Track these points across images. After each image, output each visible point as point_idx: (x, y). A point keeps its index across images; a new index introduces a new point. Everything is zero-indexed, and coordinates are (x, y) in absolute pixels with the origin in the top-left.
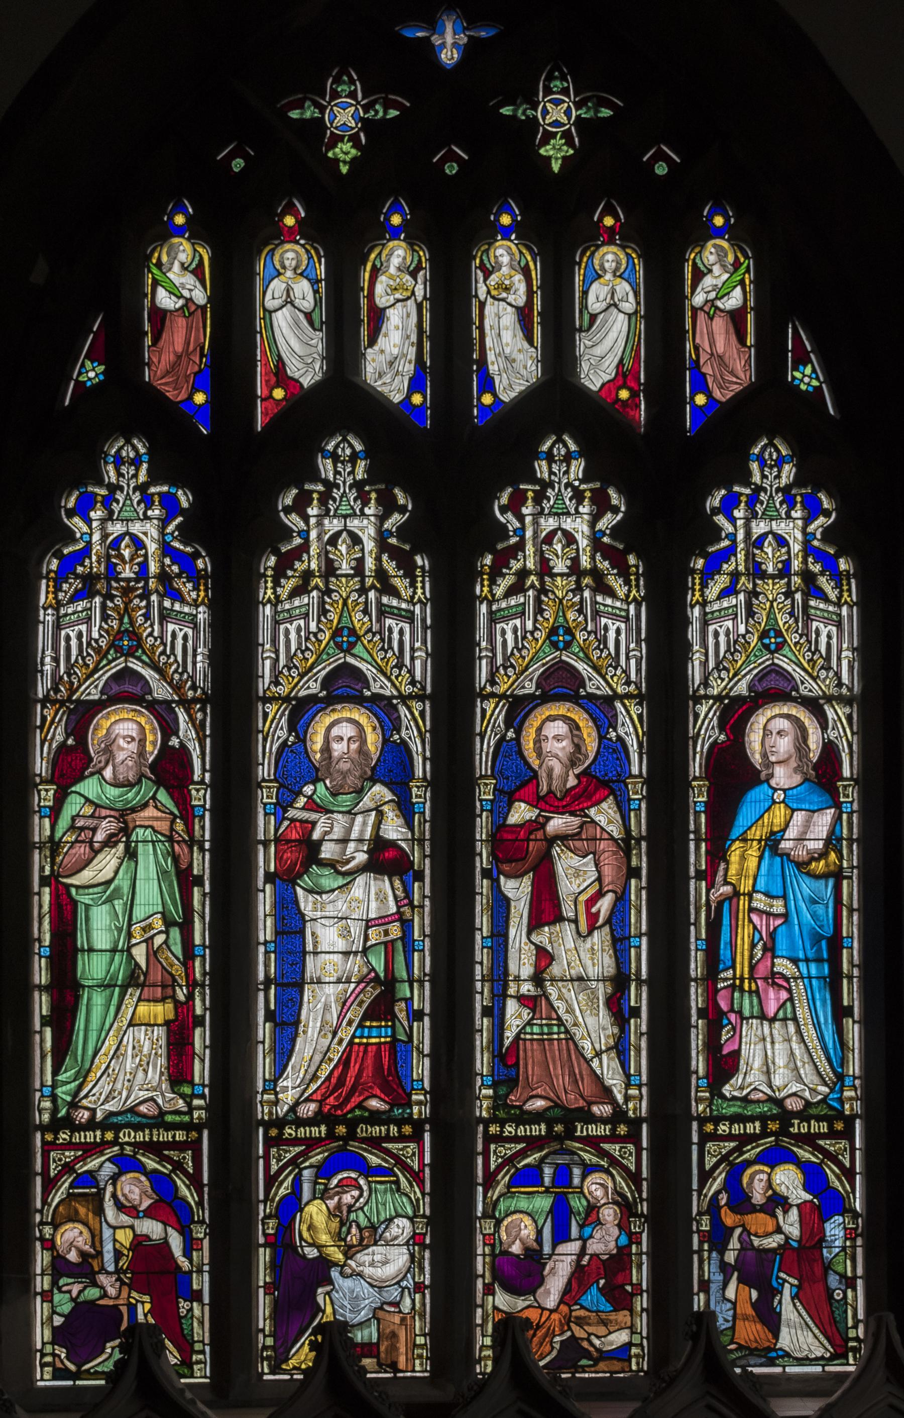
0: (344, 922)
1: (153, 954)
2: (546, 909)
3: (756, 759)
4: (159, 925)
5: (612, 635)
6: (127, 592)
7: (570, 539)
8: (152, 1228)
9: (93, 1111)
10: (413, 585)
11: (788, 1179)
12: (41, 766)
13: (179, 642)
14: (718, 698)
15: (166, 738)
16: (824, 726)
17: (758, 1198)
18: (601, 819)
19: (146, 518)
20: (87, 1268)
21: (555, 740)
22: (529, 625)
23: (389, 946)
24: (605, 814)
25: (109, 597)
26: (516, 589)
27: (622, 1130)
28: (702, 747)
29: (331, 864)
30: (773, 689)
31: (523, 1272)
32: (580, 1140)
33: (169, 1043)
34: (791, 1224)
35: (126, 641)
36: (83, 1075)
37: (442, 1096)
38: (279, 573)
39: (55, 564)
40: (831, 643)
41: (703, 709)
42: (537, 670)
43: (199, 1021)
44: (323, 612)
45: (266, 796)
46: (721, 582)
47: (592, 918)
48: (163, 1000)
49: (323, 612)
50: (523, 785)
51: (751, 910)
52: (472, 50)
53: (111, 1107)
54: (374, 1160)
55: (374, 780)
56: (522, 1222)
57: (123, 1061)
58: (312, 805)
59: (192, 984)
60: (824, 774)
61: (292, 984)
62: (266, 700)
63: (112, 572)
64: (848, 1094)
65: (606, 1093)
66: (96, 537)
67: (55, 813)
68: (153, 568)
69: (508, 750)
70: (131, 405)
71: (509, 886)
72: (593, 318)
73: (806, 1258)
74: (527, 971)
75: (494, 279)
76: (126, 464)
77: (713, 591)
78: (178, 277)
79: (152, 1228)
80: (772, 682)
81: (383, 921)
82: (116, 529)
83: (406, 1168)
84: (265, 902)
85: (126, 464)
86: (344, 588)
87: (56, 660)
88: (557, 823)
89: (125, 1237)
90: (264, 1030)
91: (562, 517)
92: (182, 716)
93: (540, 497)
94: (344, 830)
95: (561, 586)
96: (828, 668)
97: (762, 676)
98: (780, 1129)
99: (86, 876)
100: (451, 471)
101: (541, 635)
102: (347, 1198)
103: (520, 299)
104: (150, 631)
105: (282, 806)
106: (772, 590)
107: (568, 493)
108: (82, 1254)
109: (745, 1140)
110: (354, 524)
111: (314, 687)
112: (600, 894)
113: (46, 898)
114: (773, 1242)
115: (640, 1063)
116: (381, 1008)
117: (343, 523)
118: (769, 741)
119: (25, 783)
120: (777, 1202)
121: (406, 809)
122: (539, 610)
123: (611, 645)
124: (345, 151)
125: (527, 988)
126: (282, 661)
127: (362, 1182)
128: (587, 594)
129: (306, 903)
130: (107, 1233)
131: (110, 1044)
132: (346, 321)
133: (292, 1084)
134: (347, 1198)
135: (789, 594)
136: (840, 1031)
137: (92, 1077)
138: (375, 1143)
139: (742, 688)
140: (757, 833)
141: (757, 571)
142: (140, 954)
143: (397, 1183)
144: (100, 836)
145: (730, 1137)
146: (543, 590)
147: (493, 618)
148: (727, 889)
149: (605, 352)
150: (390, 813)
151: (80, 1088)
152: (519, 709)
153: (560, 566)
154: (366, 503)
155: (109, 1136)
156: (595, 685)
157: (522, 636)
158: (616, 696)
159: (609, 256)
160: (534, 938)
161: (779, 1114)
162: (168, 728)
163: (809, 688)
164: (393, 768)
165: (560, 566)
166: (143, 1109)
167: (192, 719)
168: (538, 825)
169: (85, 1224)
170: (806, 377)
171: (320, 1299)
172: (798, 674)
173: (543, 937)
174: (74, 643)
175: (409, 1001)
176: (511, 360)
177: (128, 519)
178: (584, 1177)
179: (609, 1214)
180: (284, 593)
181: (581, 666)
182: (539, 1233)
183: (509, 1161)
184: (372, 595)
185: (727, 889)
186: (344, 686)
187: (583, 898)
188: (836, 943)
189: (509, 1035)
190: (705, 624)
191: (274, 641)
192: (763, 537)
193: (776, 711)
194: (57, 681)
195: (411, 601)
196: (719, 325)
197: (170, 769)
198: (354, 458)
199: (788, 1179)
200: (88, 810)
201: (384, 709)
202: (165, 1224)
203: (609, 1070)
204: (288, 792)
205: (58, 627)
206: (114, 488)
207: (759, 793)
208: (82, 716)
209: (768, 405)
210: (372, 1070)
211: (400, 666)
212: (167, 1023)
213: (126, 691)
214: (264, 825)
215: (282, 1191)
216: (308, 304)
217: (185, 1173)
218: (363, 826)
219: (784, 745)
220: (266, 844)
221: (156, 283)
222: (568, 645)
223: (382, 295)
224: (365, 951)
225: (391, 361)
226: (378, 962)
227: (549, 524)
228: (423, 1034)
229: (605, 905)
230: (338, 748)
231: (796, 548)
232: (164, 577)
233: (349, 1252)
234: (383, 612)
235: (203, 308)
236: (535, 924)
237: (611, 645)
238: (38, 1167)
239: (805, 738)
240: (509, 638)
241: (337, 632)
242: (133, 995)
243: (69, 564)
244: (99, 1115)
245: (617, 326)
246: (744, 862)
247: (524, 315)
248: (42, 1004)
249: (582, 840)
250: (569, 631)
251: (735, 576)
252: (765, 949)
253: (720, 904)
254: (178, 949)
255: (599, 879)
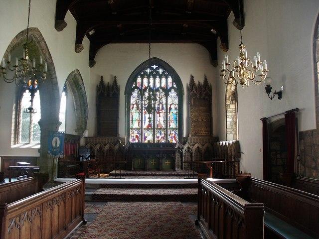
11: (173, 132)
20: (133, 137)
24: (163, 110)
30: (173, 104)
31: (158, 137)
56: (158, 135)
70: (136, 87)
73: (174, 137)
132: (149, 82)
161: (173, 129)
170: (175, 86)
176: (158, 85)
199: (173, 132)
209: (173, 87)
210: (150, 125)
225: (151, 85)
246: (171, 114)
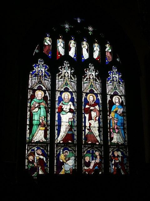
0: (66, 118)
1: (42, 121)
2: (90, 118)
3: (114, 102)
4: (43, 117)
5: (97, 86)
6: (40, 77)
7: (93, 75)
8: (42, 157)
9: (34, 141)
10: (75, 79)
11: (119, 153)
12: (29, 97)
13: (47, 83)
14: (110, 95)
15: (45, 95)
16: (122, 99)
17: (116, 155)
18: (97, 108)
19: (43, 68)
21: (91, 98)
22: (88, 84)
23: (72, 122)
24: (97, 107)
25: (38, 77)
26: (87, 80)
27: (100, 146)
28: (58, 96)
29: (65, 111)
31: (88, 164)
32: (95, 147)
33: (44, 132)
34: (120, 159)
35: (40, 82)
36: (33, 136)
37: (77, 140)
38: (59, 76)
39: (32, 72)
40: (121, 89)
41: (108, 96)
42: (89, 90)
43: (48, 130)
44: (64, 81)
45: (57, 103)
46: (110, 81)
47: (96, 120)
48: (43, 127)
49: (64, 81)
50: (88, 103)
51: (114, 120)
52: (81, 21)
53: (37, 140)
54: (70, 149)
55: (70, 101)
57: (39, 135)
58: (62, 104)
59: (47, 125)
60: (121, 104)
61: (60, 126)
62: (57, 91)
63: (38, 74)
64: (126, 143)
65: (98, 141)
66: (37, 70)
67: (30, 103)
68: (44, 74)
69: (86, 99)
71: (86, 115)
72: (95, 51)
74: (88, 126)
75: (84, 46)
76: (41, 62)
77: (109, 83)
78: (48, 41)
79: (42, 157)
80: (116, 93)
81: (71, 118)
82: (39, 69)
83: (74, 150)
84: (57, 115)
85: (41, 62)
86: (67, 78)
87: (31, 84)
88: (92, 108)
89: (38, 158)
90: (56, 132)
91: (91, 73)
92: (47, 92)
93: (89, 70)
94: (66, 108)
95: (92, 80)
96: (122, 92)
97: (115, 92)
98: (118, 146)
99: (34, 111)
100: (79, 67)
101: (89, 86)
102: (66, 154)
103: (87, 48)
104: (43, 81)
105: (59, 103)
106: (115, 83)
107: (92, 70)
108: (32, 160)
109: (114, 148)
110: (68, 71)
111: (63, 90)
112: (97, 117)
113: (29, 113)
114: (118, 161)
115: (102, 138)
116: (70, 130)
117: (66, 71)
118: (116, 100)
119: (27, 99)
120: (118, 156)
121: (74, 105)
122: (89, 83)
123: (97, 87)
124: (67, 30)
125: (88, 128)
126: (59, 86)
127: (68, 152)
128: (95, 81)
129: (61, 115)
130: (35, 157)
131: (37, 132)
133: (59, 139)
134: (66, 154)
135: (117, 83)
136: (125, 135)
137: (34, 137)
138: (70, 147)
139: (112, 94)
140: (114, 110)
141: (113, 80)
142: (41, 121)
143: (73, 152)
144: (36, 106)
145: (113, 148)
146: (89, 81)
147: (84, 83)
148: (111, 117)
149: (96, 55)
150: (72, 105)
151: (33, 138)
152: (87, 94)
153: (91, 78)
154: (69, 69)
155: (36, 144)
156: (96, 92)
157: (87, 86)
158: (98, 93)
159: (60, 40)
160: (89, 122)
162: (45, 93)
163: (120, 94)
164: (72, 100)
165: (91, 78)
166: (41, 141)
167: (48, 92)
168: (89, 108)
169: (33, 156)
171: (63, 167)
172: (118, 93)
173: (90, 121)
174: (34, 82)
175: (74, 129)
176: (86, 55)
177: (41, 68)
178: (95, 152)
179: (98, 157)
180: (59, 78)
181: (94, 90)
182: (90, 159)
183: (87, 150)
184: (70, 79)
185: (111, 117)
186: (66, 90)
187: (95, 117)
188: (124, 124)
189: (86, 134)
190: (108, 86)
191: (58, 84)
192: (114, 77)
193: (116, 96)
194: (31, 86)
195: (74, 80)
196: (108, 53)
197: (45, 98)
198: (68, 64)
199: (119, 153)
200: (35, 102)
201: (71, 93)
202: (43, 156)
203: (98, 138)
204: (59, 102)
205: (32, 80)
206: (39, 64)
207: (115, 106)
208: (34, 91)
210: (68, 136)
211: (73, 88)
212: (44, 130)
213: (40, 89)
214: (57, 106)
215: (58, 153)
216: (63, 46)
217: (46, 150)
218: (68, 107)
219: (117, 101)
220: (57, 108)
221: (45, 42)
222: (92, 87)
223: (71, 46)
224: (69, 122)
226: (70, 123)
227: (90, 73)
228: (76, 133)
229: (97, 118)
230: (66, 97)
231: (118, 78)
232: (45, 75)
233: (67, 161)
234: (71, 81)
235: (50, 45)
236: (89, 120)
237: (97, 87)
238: (27, 148)
239: (119, 99)
240: (86, 86)
241: (65, 83)
242: (40, 126)
243: (33, 73)
244: (35, 142)
245: (97, 53)
247: (87, 50)
248: (28, 127)
249: (95, 110)
250: (92, 85)
251: (87, 79)
252: (116, 125)
253: (111, 119)
254: (46, 121)
255: (96, 115)
